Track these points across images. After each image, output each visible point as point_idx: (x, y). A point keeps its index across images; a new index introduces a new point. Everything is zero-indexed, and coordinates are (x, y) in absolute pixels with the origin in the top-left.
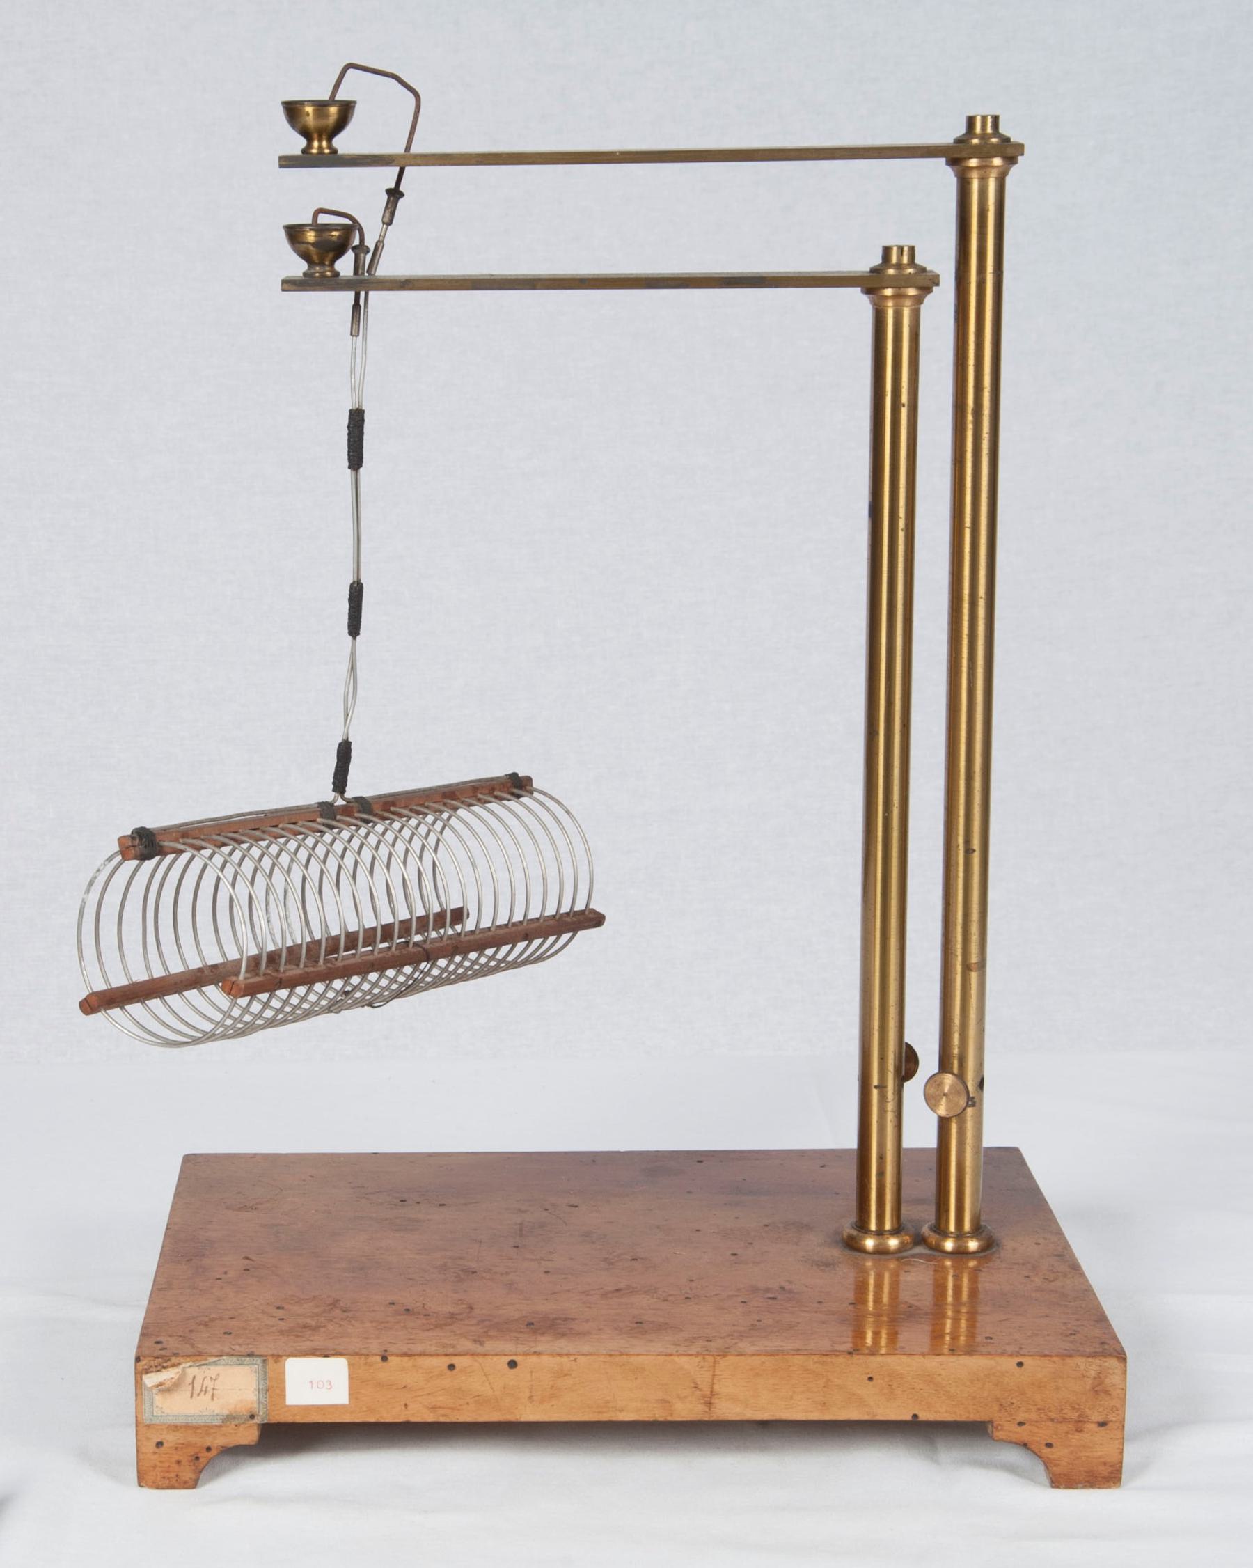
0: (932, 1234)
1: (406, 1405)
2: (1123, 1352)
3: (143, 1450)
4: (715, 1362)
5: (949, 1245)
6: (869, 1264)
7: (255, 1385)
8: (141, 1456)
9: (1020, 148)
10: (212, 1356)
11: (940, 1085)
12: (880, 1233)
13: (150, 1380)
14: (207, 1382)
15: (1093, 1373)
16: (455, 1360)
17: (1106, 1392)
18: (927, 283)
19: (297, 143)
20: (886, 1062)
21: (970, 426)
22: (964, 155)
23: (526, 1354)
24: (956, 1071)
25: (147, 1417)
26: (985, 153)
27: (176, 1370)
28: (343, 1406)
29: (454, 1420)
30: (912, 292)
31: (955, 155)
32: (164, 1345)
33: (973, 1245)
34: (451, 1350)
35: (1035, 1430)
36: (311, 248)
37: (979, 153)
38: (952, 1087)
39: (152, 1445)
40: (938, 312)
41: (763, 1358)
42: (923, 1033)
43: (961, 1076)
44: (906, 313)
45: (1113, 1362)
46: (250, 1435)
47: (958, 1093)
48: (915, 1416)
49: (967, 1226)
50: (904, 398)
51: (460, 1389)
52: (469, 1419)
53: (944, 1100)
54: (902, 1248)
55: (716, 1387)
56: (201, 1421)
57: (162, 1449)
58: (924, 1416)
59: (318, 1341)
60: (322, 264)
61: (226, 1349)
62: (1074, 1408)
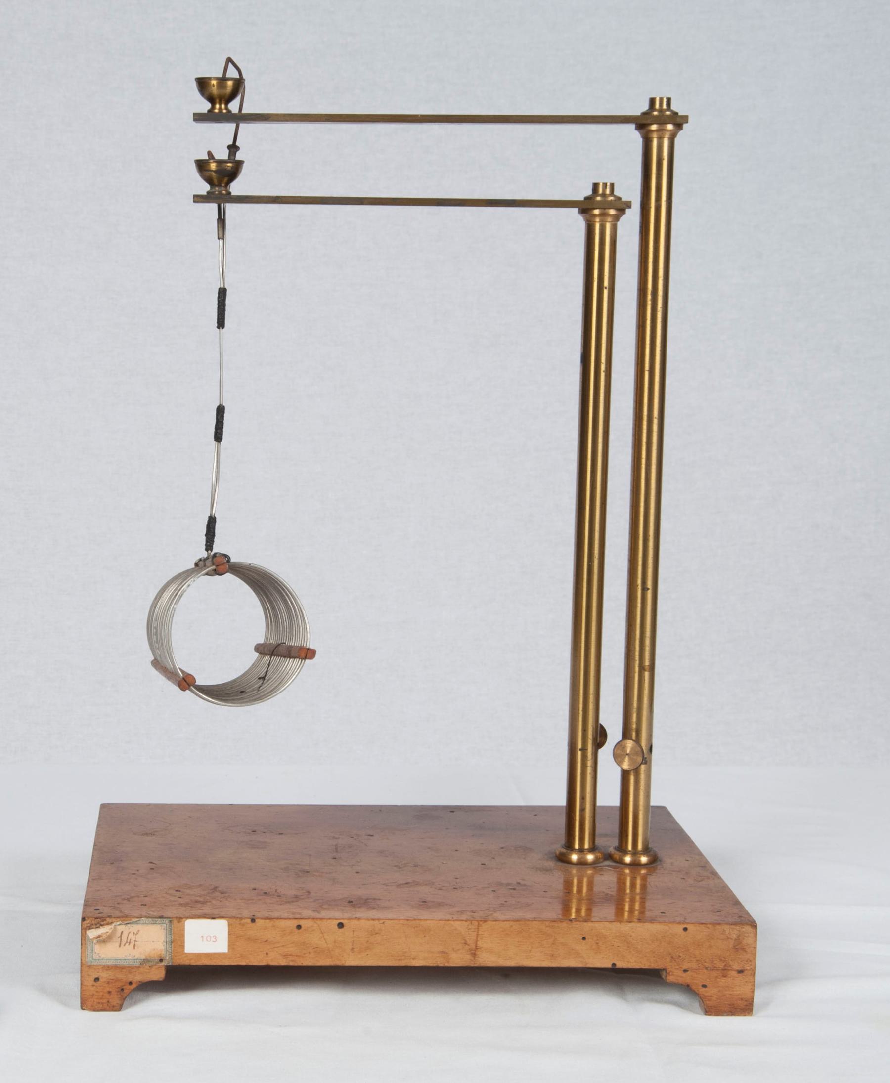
0: (617, 853)
1: (267, 954)
2: (754, 922)
3: (85, 983)
4: (479, 925)
5: (628, 859)
6: (574, 872)
7: (163, 939)
8: (84, 988)
9: (685, 119)
10: (135, 917)
11: (624, 748)
12: (581, 850)
13: (92, 934)
14: (131, 936)
15: (735, 936)
16: (301, 923)
17: (744, 950)
18: (622, 207)
19: (204, 106)
20: (586, 737)
21: (649, 303)
22: (649, 121)
23: (349, 919)
24: (634, 738)
25: (89, 960)
26: (662, 121)
27: (110, 927)
28: (224, 954)
29: (300, 964)
30: (612, 212)
31: (642, 123)
32: (101, 911)
33: (644, 859)
34: (298, 916)
35: (695, 975)
36: (213, 174)
37: (656, 122)
38: (632, 749)
39: (91, 980)
40: (630, 221)
41: (512, 923)
42: (611, 716)
43: (638, 741)
44: (608, 227)
45: (748, 929)
46: (158, 974)
47: (637, 754)
48: (614, 965)
49: (640, 847)
50: (606, 283)
51: (304, 943)
52: (310, 964)
53: (627, 759)
54: (595, 862)
55: (479, 943)
56: (126, 964)
57: (98, 983)
58: (620, 965)
59: (207, 909)
60: (219, 185)
61: (144, 914)
62: (721, 960)
